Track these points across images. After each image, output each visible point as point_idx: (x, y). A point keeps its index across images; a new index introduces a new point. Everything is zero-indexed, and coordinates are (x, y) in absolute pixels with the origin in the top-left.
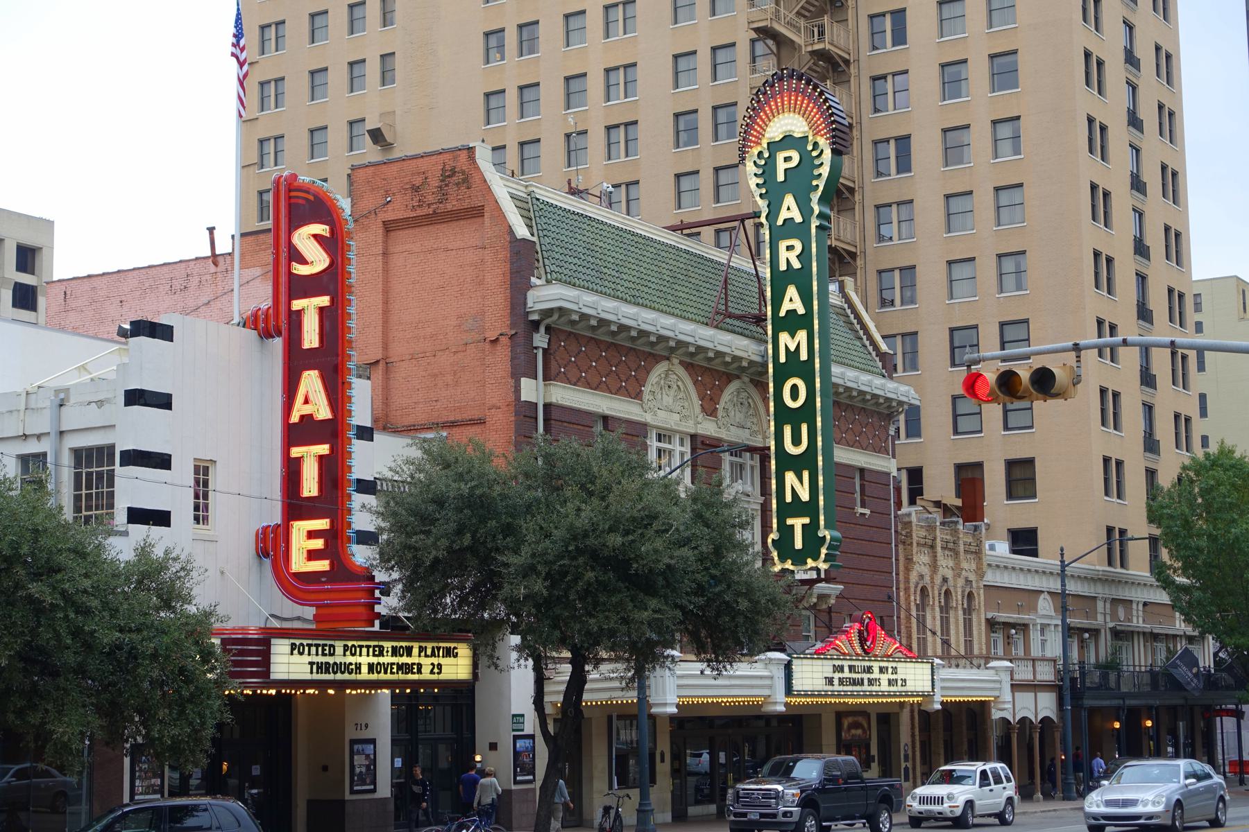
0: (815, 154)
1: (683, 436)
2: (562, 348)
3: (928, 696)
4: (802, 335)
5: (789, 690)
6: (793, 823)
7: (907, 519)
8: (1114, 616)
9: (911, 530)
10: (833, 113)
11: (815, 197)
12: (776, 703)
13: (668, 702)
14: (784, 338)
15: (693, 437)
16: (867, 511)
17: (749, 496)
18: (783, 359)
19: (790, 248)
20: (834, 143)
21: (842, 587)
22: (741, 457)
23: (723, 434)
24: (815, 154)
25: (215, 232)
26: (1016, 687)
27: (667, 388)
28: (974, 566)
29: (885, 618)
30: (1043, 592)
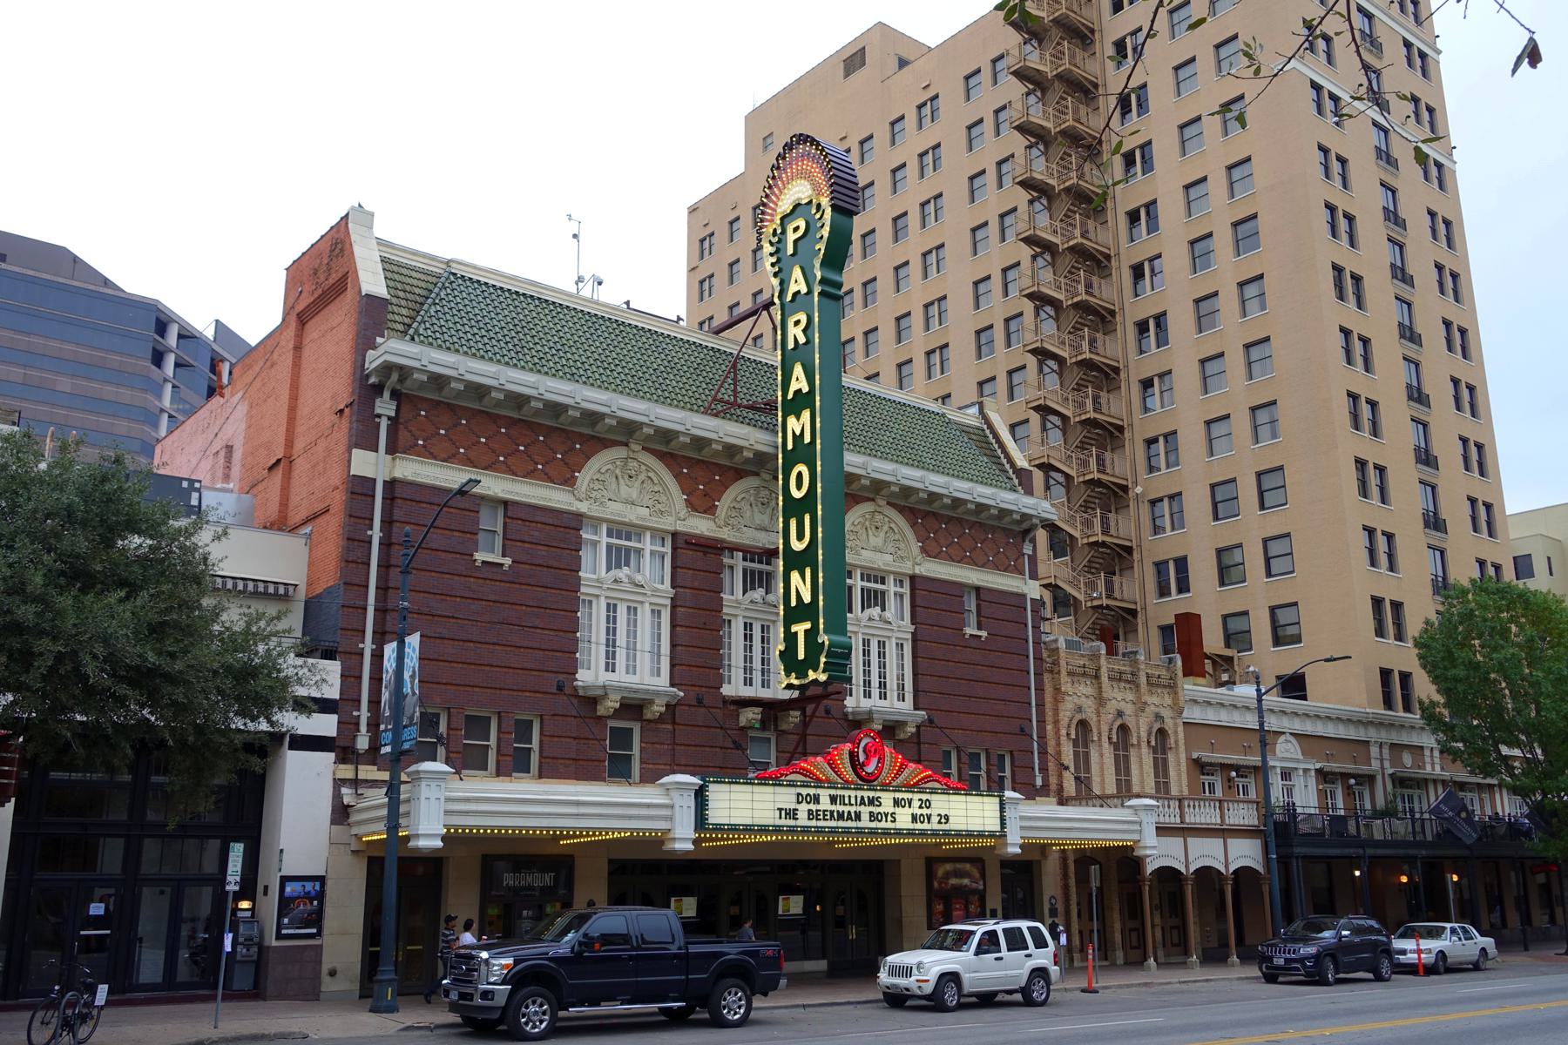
1: (663, 535)
2: (423, 418)
6: (498, 1008)
7: (1054, 646)
8: (1396, 761)
11: (817, 264)
12: (1146, 847)
13: (677, 836)
14: (791, 421)
16: (984, 634)
18: (790, 446)
20: (832, 199)
23: (726, 534)
24: (818, 216)
26: (1162, 830)
30: (1284, 733)
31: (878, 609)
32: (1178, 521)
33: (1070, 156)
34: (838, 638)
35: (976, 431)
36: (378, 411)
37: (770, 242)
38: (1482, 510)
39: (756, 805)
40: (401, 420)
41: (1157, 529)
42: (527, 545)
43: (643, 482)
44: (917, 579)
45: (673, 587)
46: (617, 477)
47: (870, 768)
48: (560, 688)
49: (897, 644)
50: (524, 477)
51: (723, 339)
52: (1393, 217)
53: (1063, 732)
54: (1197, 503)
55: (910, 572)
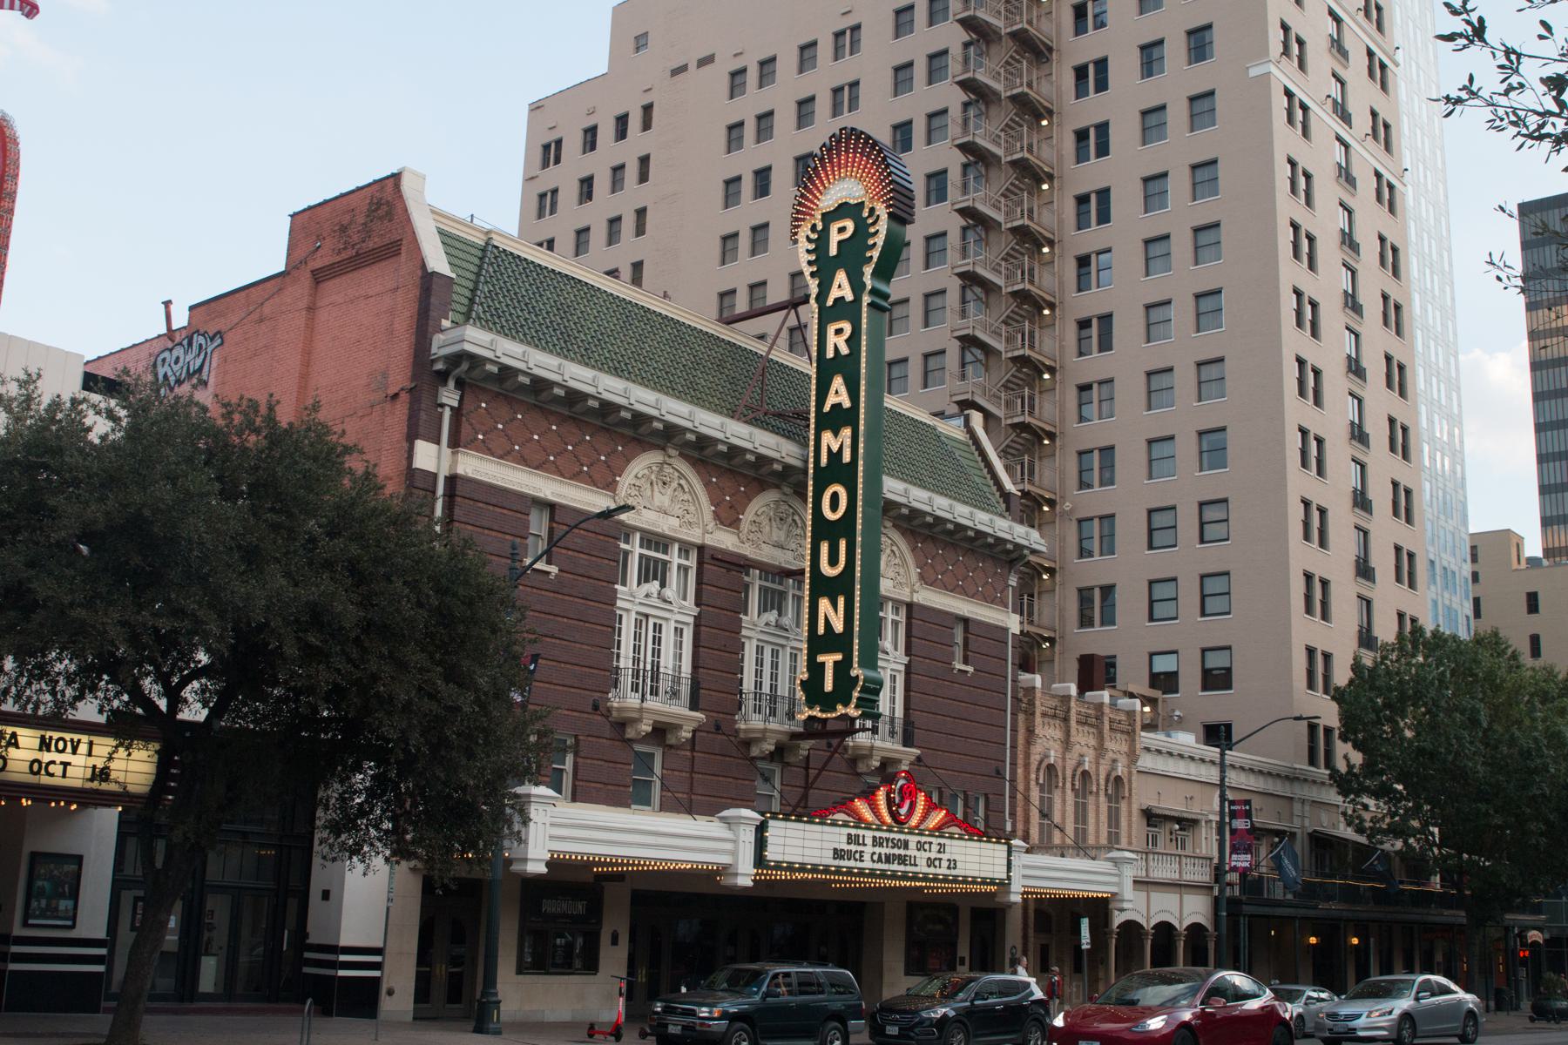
0: (870, 221)
2: (483, 411)
3: (1004, 885)
4: (847, 432)
5: (760, 860)
9: (1034, 698)
10: (891, 172)
11: (868, 270)
14: (827, 437)
15: (701, 549)
16: (970, 669)
17: (787, 630)
19: (839, 332)
21: (919, 752)
22: (781, 584)
23: (748, 551)
24: (870, 221)
25: (173, 308)
27: (660, 484)
28: (1125, 748)
29: (991, 796)
31: (656, 584)
32: (1108, 547)
33: (1021, 126)
34: (871, 674)
35: (962, 447)
36: (444, 400)
37: (808, 237)
38: (1316, 515)
39: (977, 859)
40: (464, 412)
41: (1084, 552)
42: (570, 553)
43: (675, 490)
44: (915, 608)
45: (697, 604)
46: (651, 484)
47: (903, 811)
48: (596, 708)
49: (676, 629)
50: (570, 479)
51: (734, 330)
52: (1349, 241)
53: (1033, 776)
54: (1131, 529)
55: (908, 600)
